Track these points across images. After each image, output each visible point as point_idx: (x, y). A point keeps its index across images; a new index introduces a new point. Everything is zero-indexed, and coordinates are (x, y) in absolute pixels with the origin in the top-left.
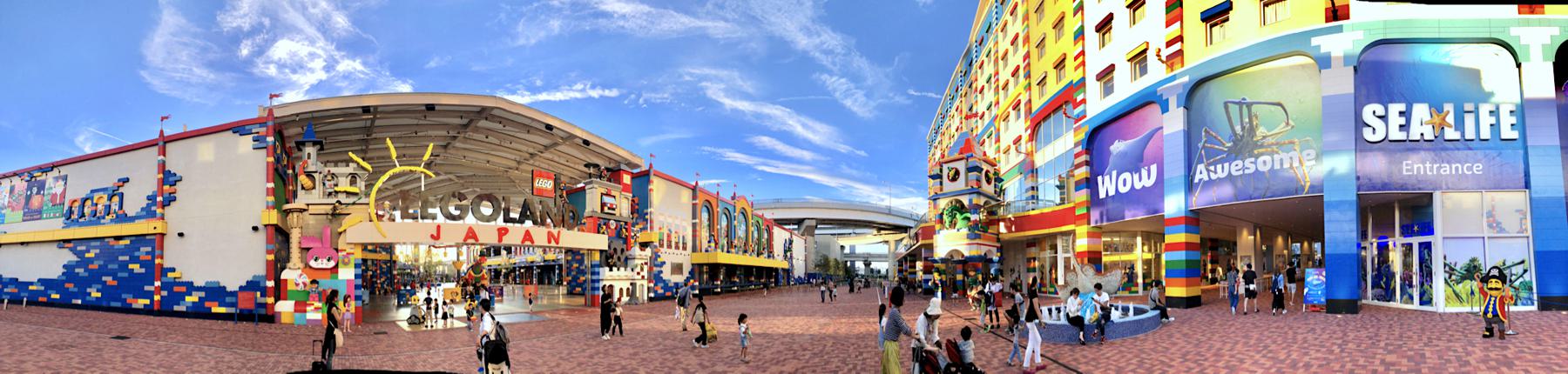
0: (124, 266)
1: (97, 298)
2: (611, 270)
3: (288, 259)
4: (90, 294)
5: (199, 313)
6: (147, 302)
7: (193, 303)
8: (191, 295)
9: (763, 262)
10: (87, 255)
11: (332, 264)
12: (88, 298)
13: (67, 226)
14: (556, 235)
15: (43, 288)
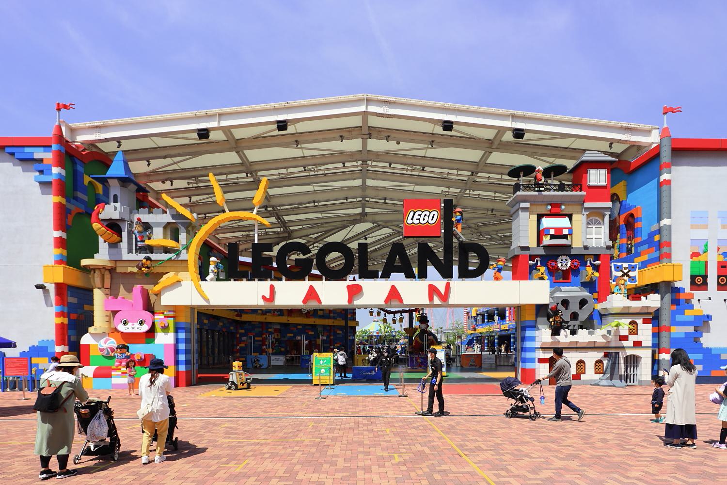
3: (89, 321)
11: (145, 328)
14: (443, 291)
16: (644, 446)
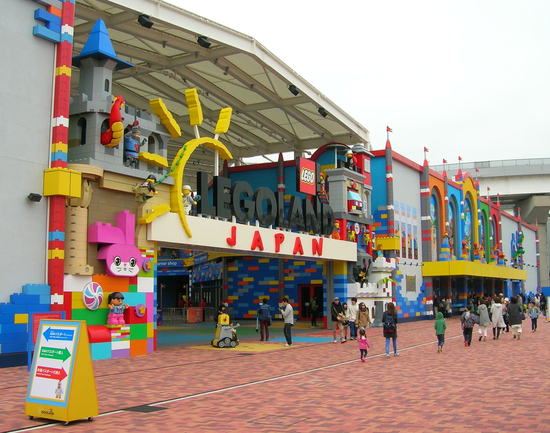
2: (362, 287)
7: (244, 293)
16: (463, 375)
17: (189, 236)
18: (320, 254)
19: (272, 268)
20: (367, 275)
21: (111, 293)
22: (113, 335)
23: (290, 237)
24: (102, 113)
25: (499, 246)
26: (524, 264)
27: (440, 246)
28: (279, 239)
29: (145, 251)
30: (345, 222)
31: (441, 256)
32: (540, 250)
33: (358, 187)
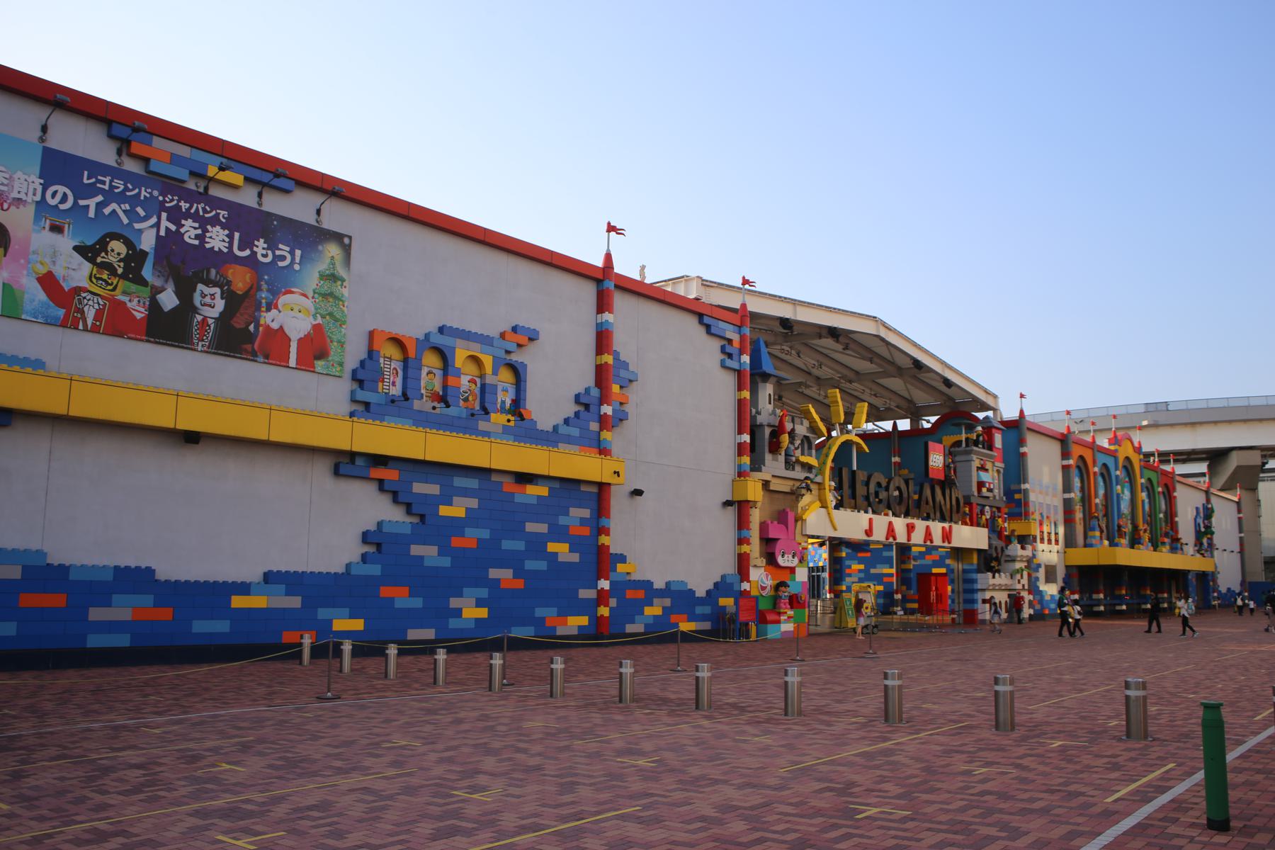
0: (536, 546)
1: (478, 620)
2: (994, 577)
4: (458, 613)
5: (661, 636)
6: (584, 620)
8: (651, 604)
9: (1162, 559)
10: (444, 511)
12: (453, 623)
13: (364, 409)
15: (295, 602)
17: (835, 529)
18: (949, 543)
19: (885, 554)
20: (999, 564)
21: (778, 582)
22: (782, 618)
23: (920, 525)
24: (769, 425)
25: (1173, 526)
26: (1217, 549)
27: (1087, 529)
28: (911, 528)
29: (800, 544)
30: (974, 505)
31: (1088, 541)
32: (1245, 528)
33: (989, 466)
